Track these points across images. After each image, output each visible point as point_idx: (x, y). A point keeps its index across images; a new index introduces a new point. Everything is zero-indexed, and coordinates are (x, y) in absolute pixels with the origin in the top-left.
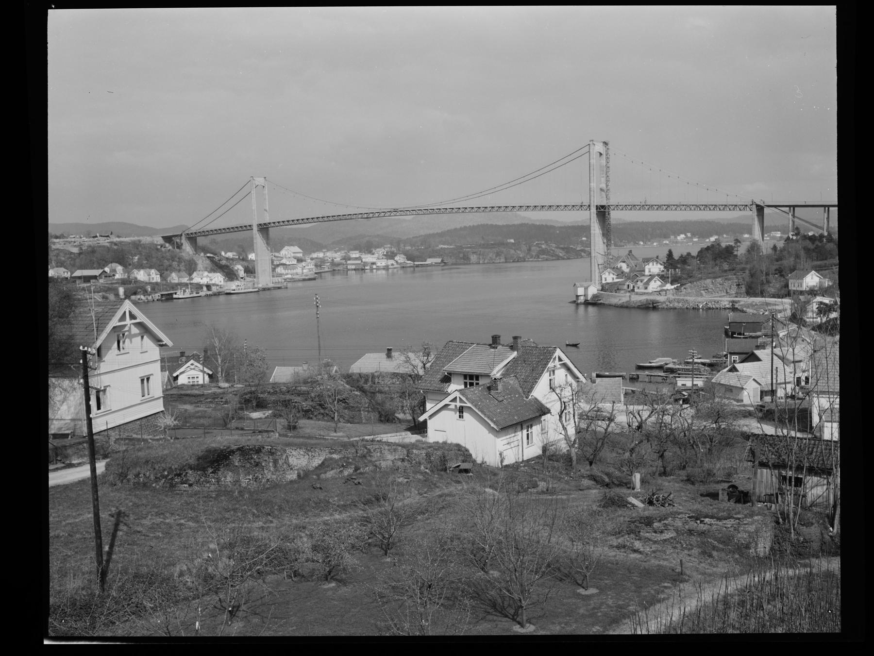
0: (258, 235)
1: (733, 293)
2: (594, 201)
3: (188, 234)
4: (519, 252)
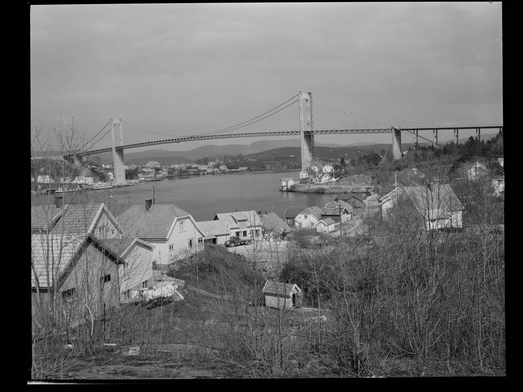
0: (116, 154)
1: (370, 183)
2: (302, 129)
3: (77, 154)
4: (296, 163)
